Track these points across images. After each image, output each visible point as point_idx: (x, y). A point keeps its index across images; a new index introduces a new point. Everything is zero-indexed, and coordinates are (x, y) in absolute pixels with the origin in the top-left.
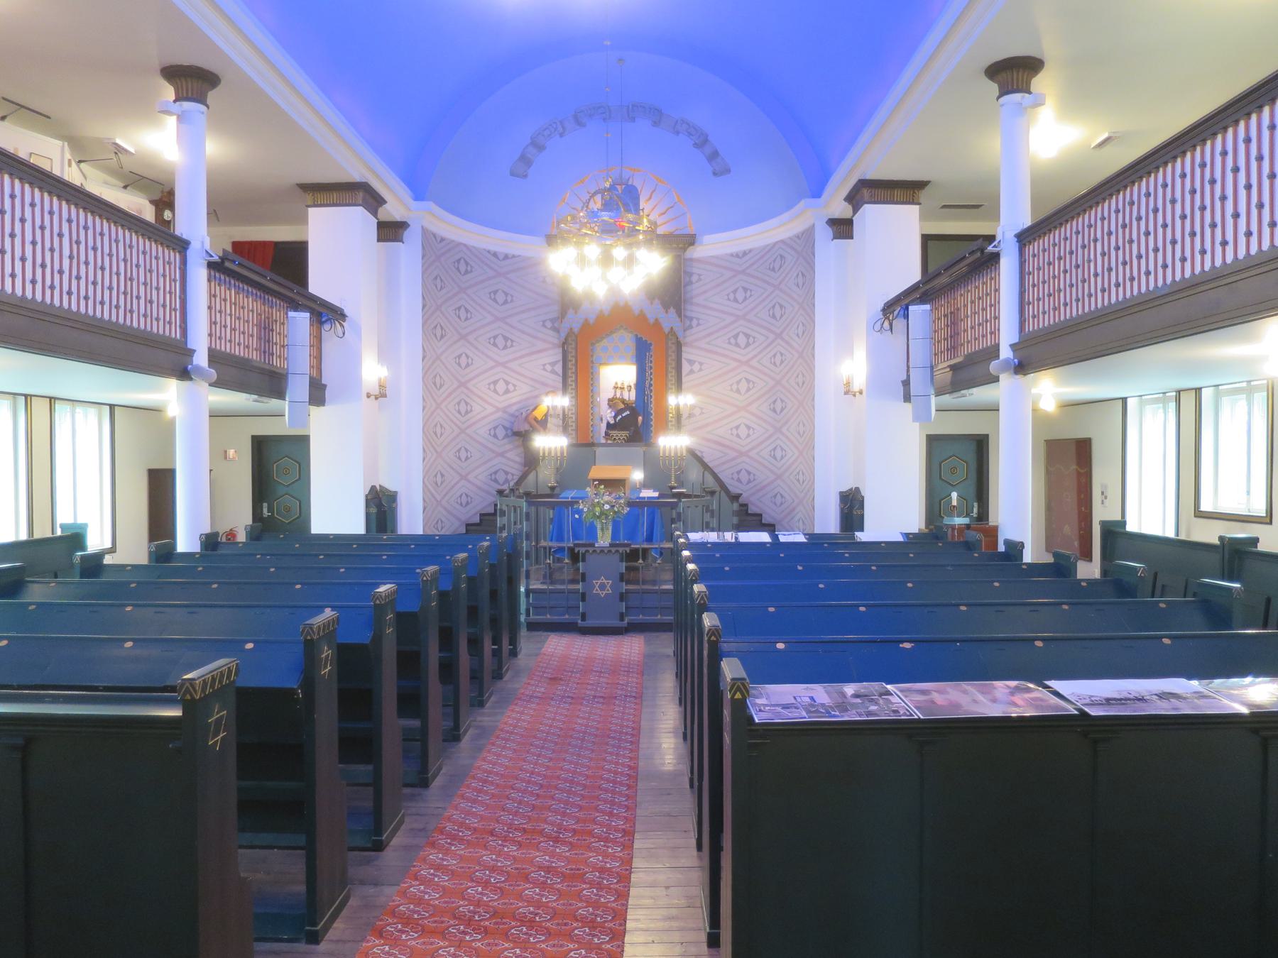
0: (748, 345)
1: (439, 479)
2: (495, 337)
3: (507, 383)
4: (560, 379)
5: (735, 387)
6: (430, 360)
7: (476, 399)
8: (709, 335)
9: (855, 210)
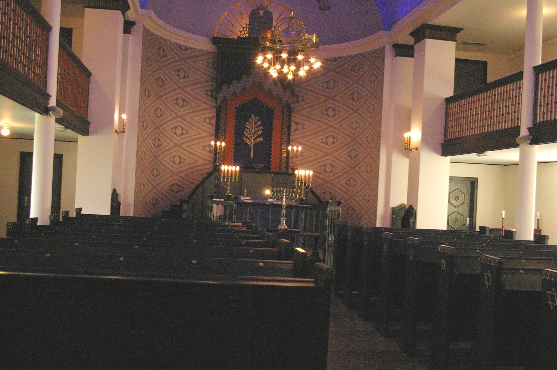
0: (334, 115)
1: (142, 188)
2: (177, 99)
3: (182, 129)
4: (214, 128)
5: (324, 141)
9: (417, 41)
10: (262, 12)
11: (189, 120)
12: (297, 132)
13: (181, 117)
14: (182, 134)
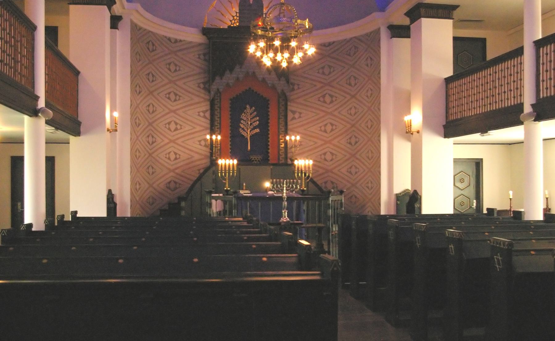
0: (332, 102)
2: (169, 93)
4: (209, 122)
5: (323, 128)
6: (134, 109)
7: (158, 133)
8: (307, 94)
12: (294, 121)
13: (174, 111)
14: (176, 129)
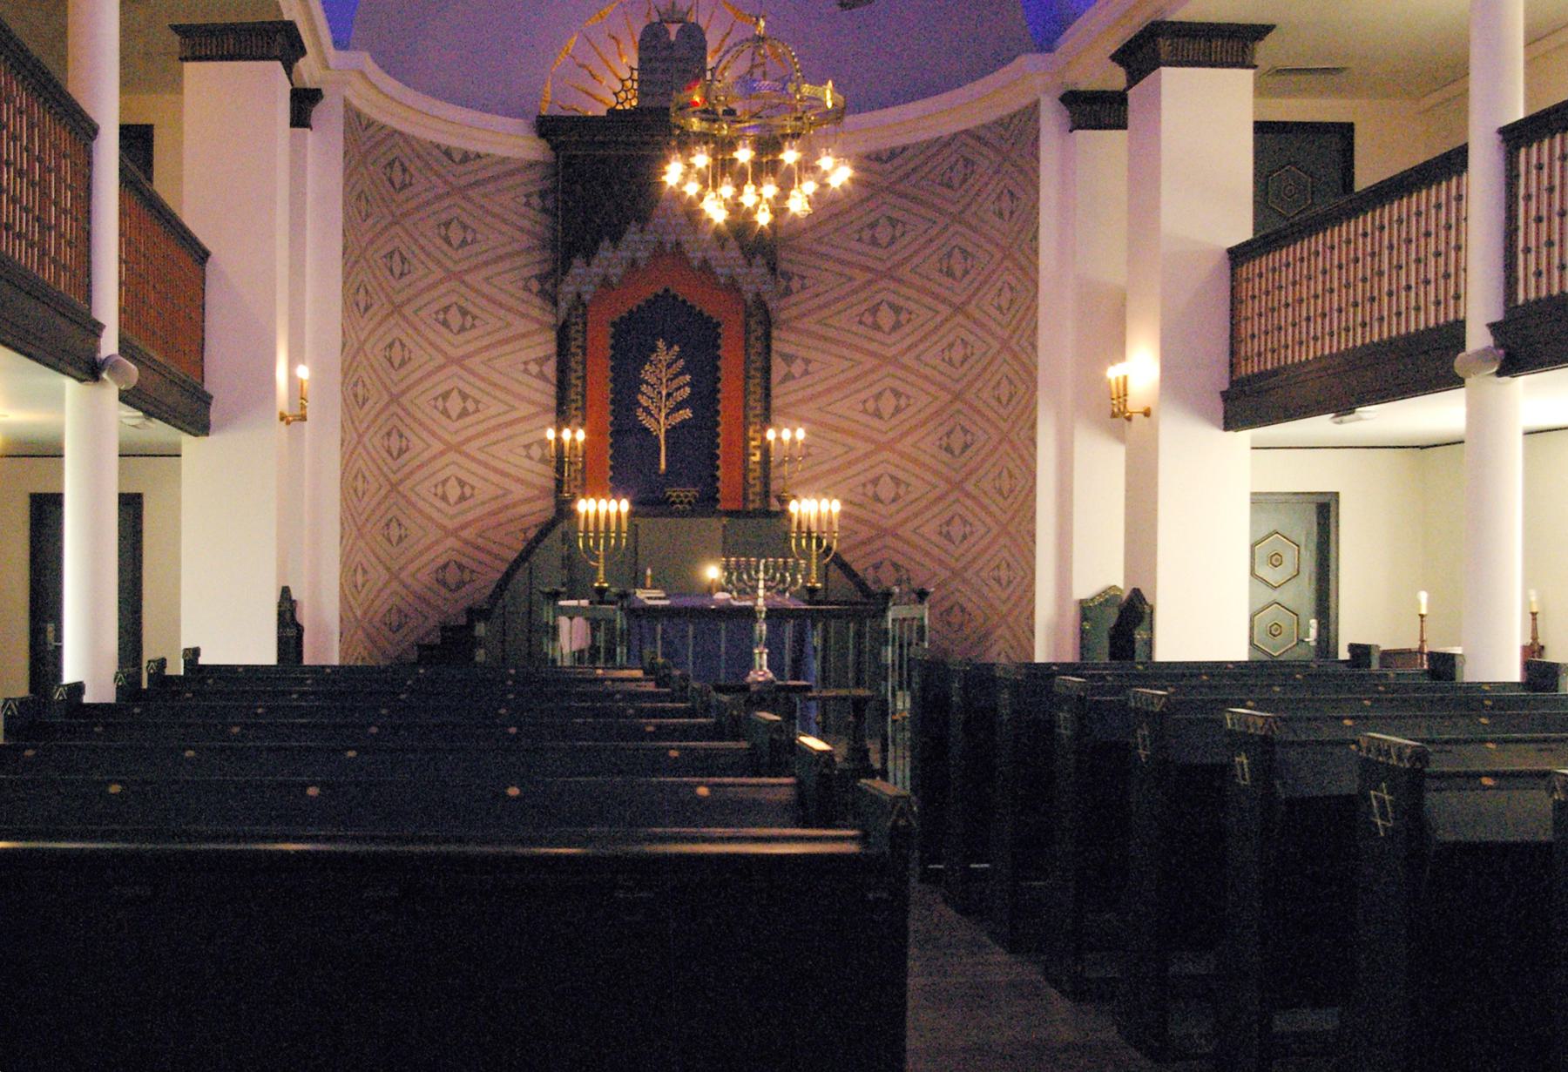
1: (360, 579)
4: (552, 390)
5: (871, 406)
10: (673, 30)
11: (482, 370)
12: (791, 385)
13: (459, 361)
14: (464, 413)
